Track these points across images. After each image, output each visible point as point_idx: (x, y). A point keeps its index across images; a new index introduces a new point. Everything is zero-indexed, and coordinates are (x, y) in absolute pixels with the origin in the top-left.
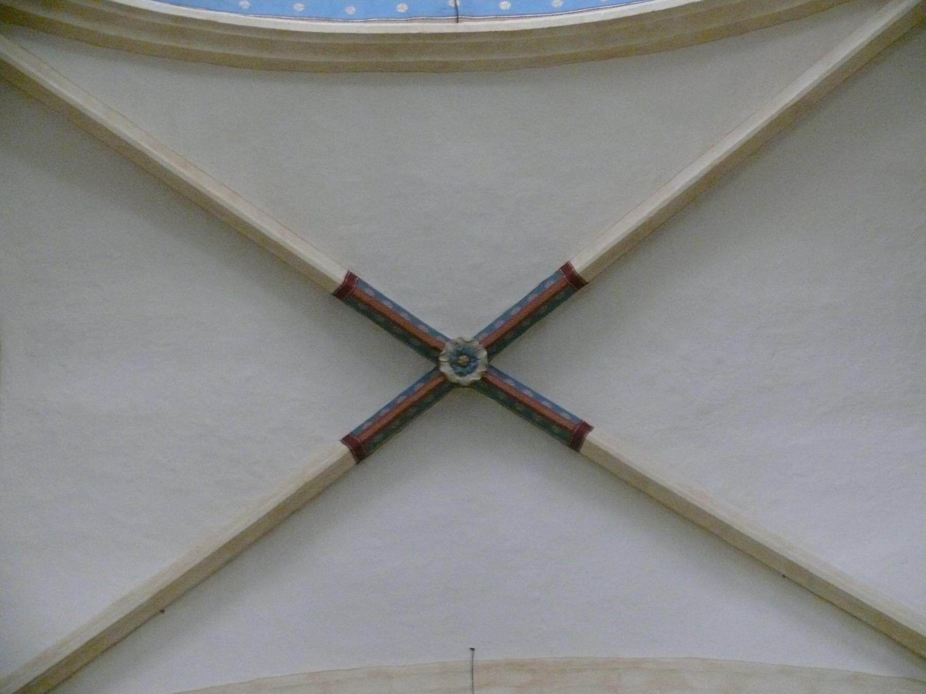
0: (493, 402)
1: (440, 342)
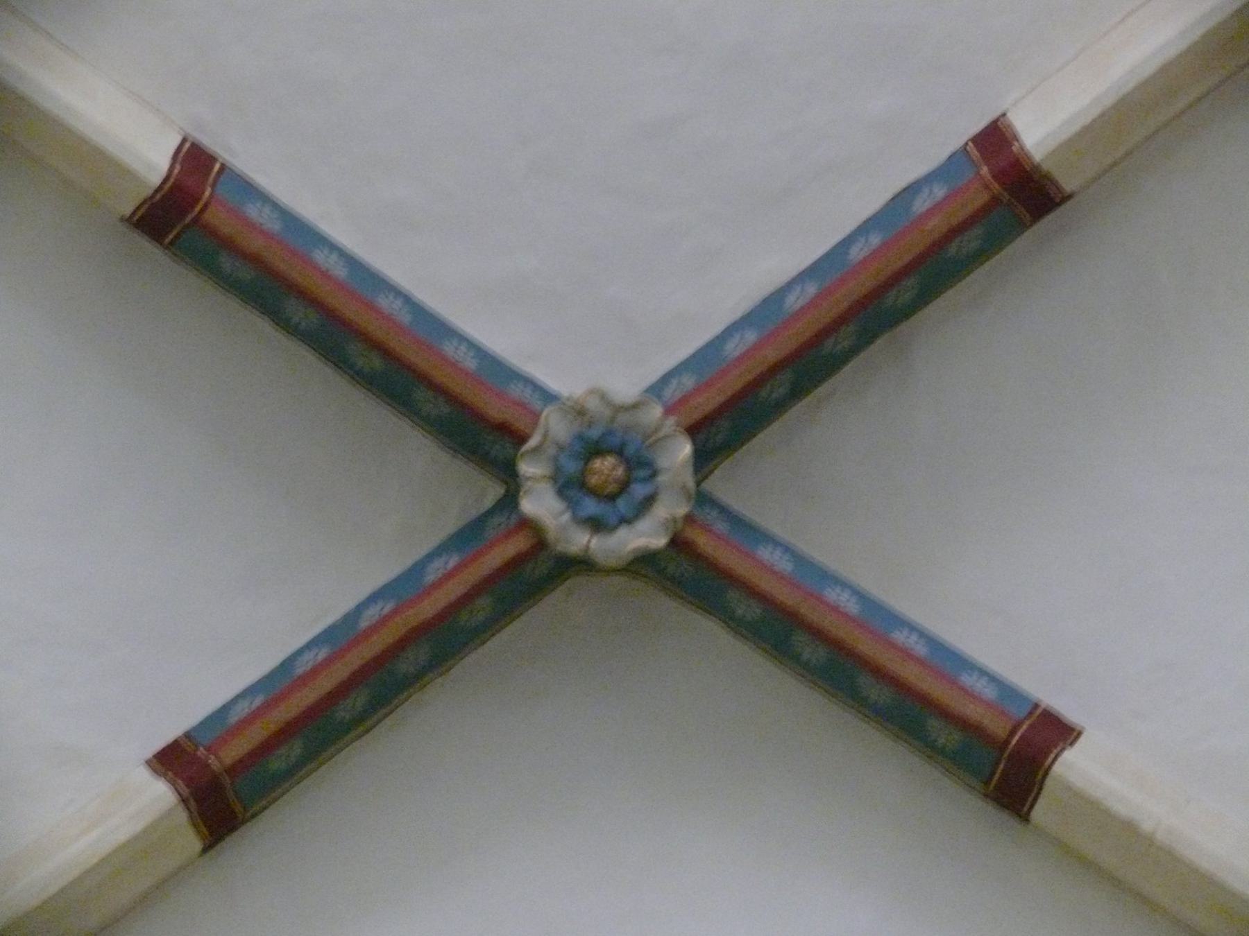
0: (709, 627)
1: (521, 405)
